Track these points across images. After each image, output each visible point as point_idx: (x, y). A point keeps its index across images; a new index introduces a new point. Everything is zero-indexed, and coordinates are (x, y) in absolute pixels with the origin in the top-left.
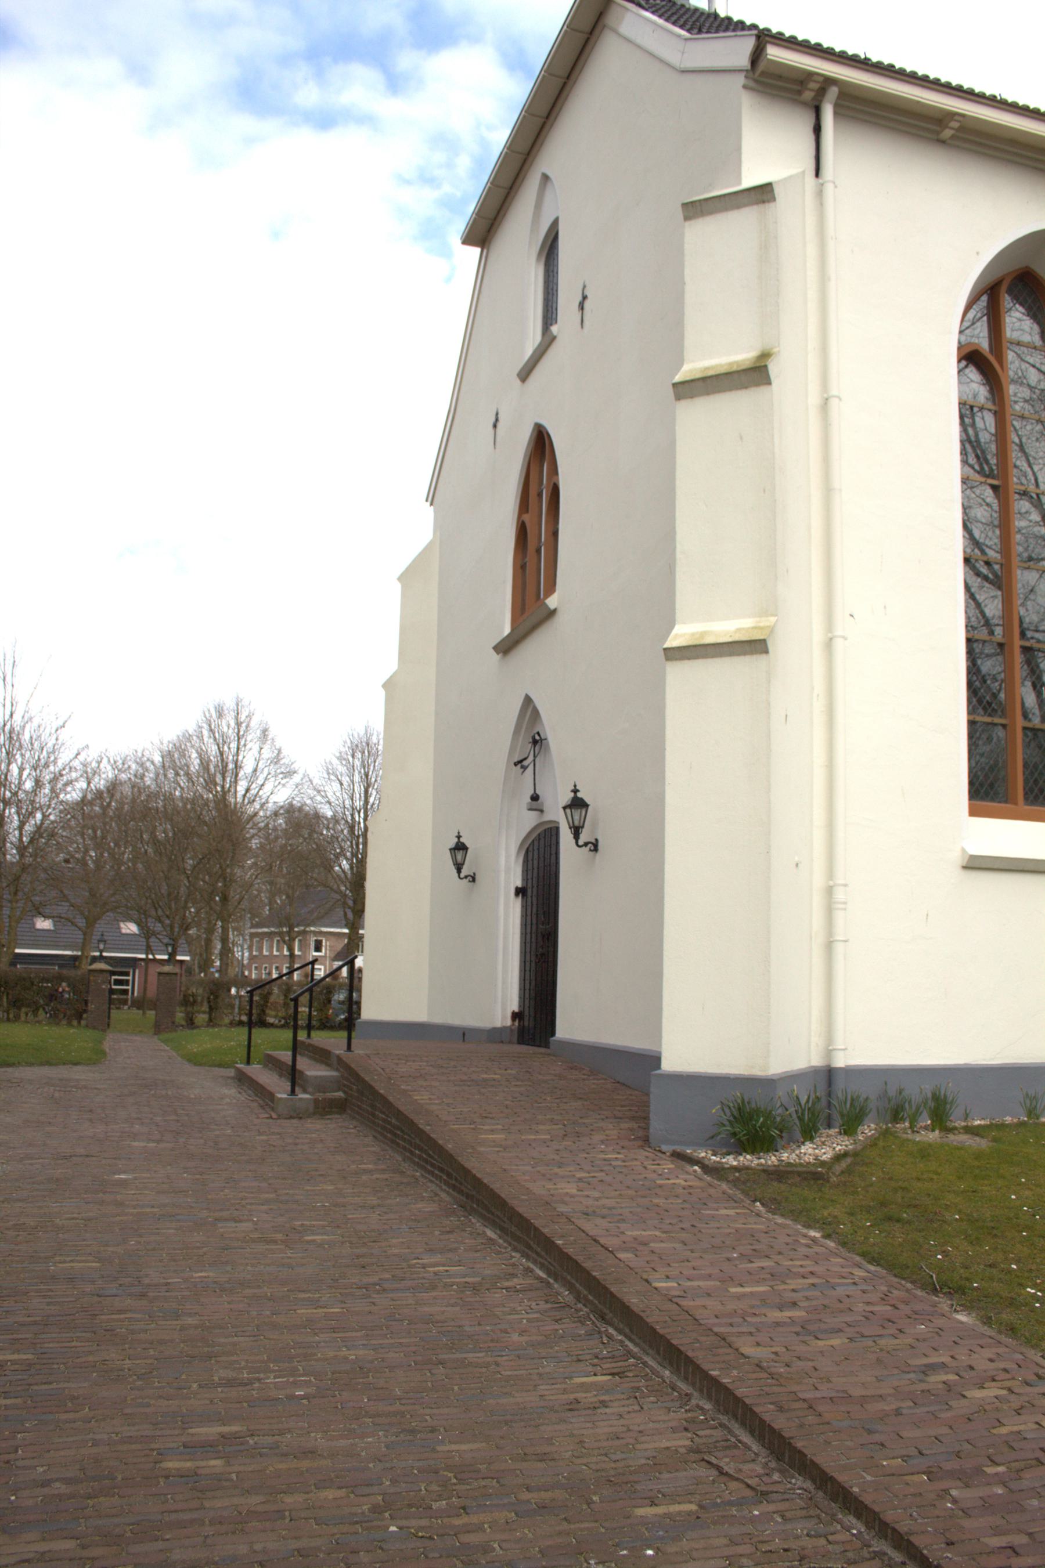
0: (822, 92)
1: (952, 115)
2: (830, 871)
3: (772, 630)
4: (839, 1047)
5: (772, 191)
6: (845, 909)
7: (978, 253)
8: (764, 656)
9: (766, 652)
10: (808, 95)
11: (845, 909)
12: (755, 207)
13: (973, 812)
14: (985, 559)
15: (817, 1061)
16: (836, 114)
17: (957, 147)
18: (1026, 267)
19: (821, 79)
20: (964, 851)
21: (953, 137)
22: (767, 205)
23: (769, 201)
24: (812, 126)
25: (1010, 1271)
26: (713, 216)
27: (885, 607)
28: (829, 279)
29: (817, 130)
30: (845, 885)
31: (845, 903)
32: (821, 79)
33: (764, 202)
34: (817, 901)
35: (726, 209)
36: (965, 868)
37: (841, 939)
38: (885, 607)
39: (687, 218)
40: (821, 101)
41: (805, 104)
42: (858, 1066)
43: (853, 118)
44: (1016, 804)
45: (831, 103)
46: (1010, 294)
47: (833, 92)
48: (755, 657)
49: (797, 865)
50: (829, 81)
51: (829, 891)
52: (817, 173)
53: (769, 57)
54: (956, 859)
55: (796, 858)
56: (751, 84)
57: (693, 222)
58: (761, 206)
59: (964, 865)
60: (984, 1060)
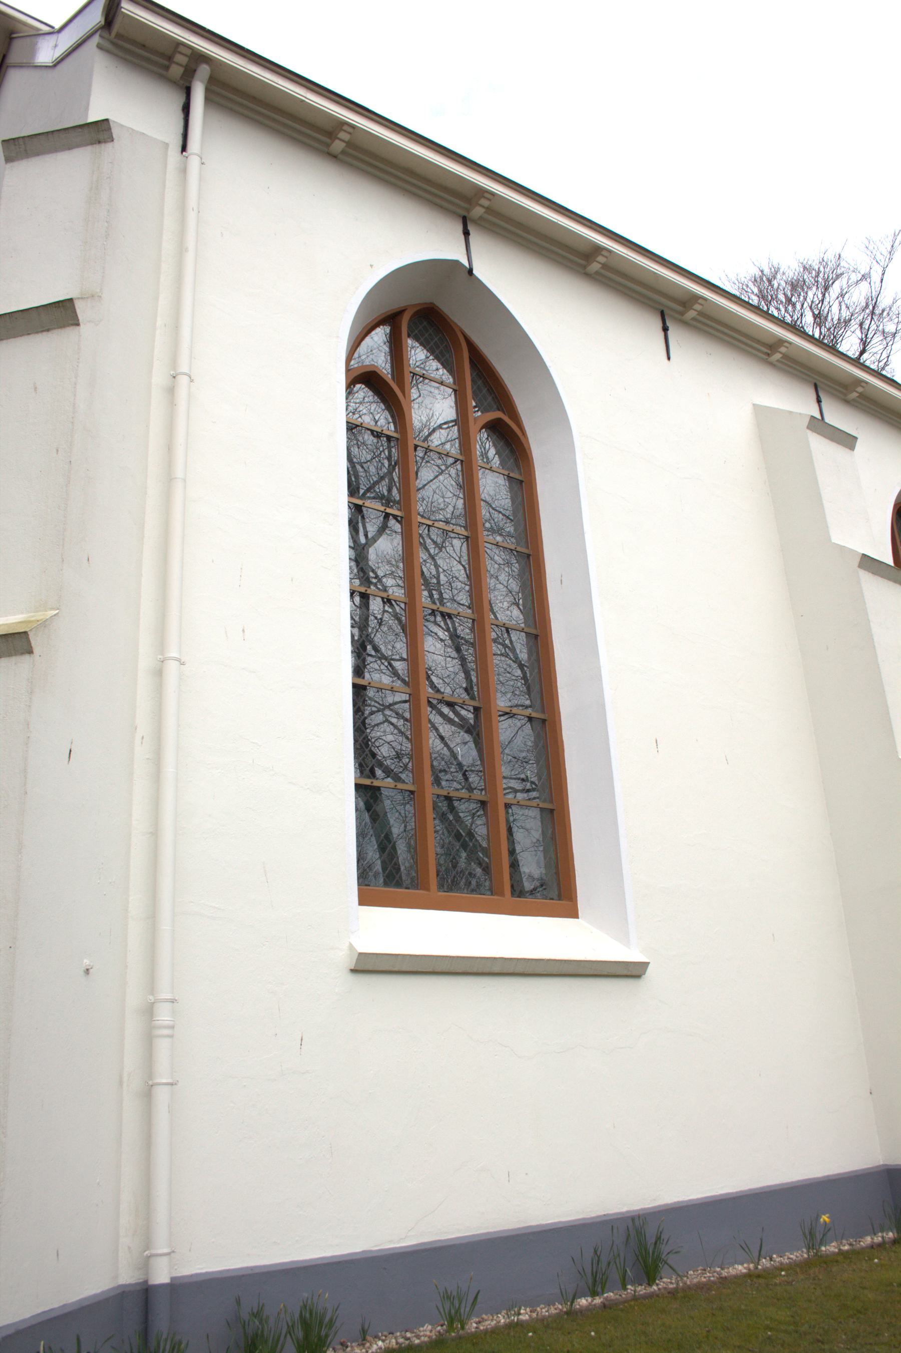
0: (189, 73)
1: (342, 124)
2: (151, 983)
3: (44, 624)
4: (160, 1251)
5: (109, 129)
6: (171, 1036)
7: (371, 266)
8: (27, 657)
9: (30, 651)
10: (176, 71)
11: (171, 1036)
12: (89, 148)
13: (365, 899)
14: (385, 595)
15: (127, 1276)
16: (208, 100)
17: (350, 166)
18: (431, 303)
19: (189, 52)
20: (351, 947)
21: (343, 152)
22: (103, 145)
23: (105, 142)
24: (181, 106)
25: (596, 1333)
26: (40, 157)
27: (243, 631)
28: (187, 250)
29: (186, 109)
30: (173, 1001)
31: (172, 1027)
32: (189, 52)
33: (99, 142)
34: (133, 1026)
35: (55, 150)
36: (354, 971)
37: (164, 1081)
38: (243, 631)
39: (8, 159)
40: (190, 82)
41: (172, 82)
42: (197, 1275)
43: (231, 110)
44: (428, 889)
45: (202, 81)
46: (416, 338)
47: (204, 70)
48: (14, 659)
49: (87, 971)
50: (200, 58)
51: (149, 1011)
52: (184, 148)
53: (123, 10)
54: (343, 959)
55: (86, 962)
56: (107, 44)
57: (15, 164)
58: (97, 146)
59: (353, 968)
60: (390, 1242)
